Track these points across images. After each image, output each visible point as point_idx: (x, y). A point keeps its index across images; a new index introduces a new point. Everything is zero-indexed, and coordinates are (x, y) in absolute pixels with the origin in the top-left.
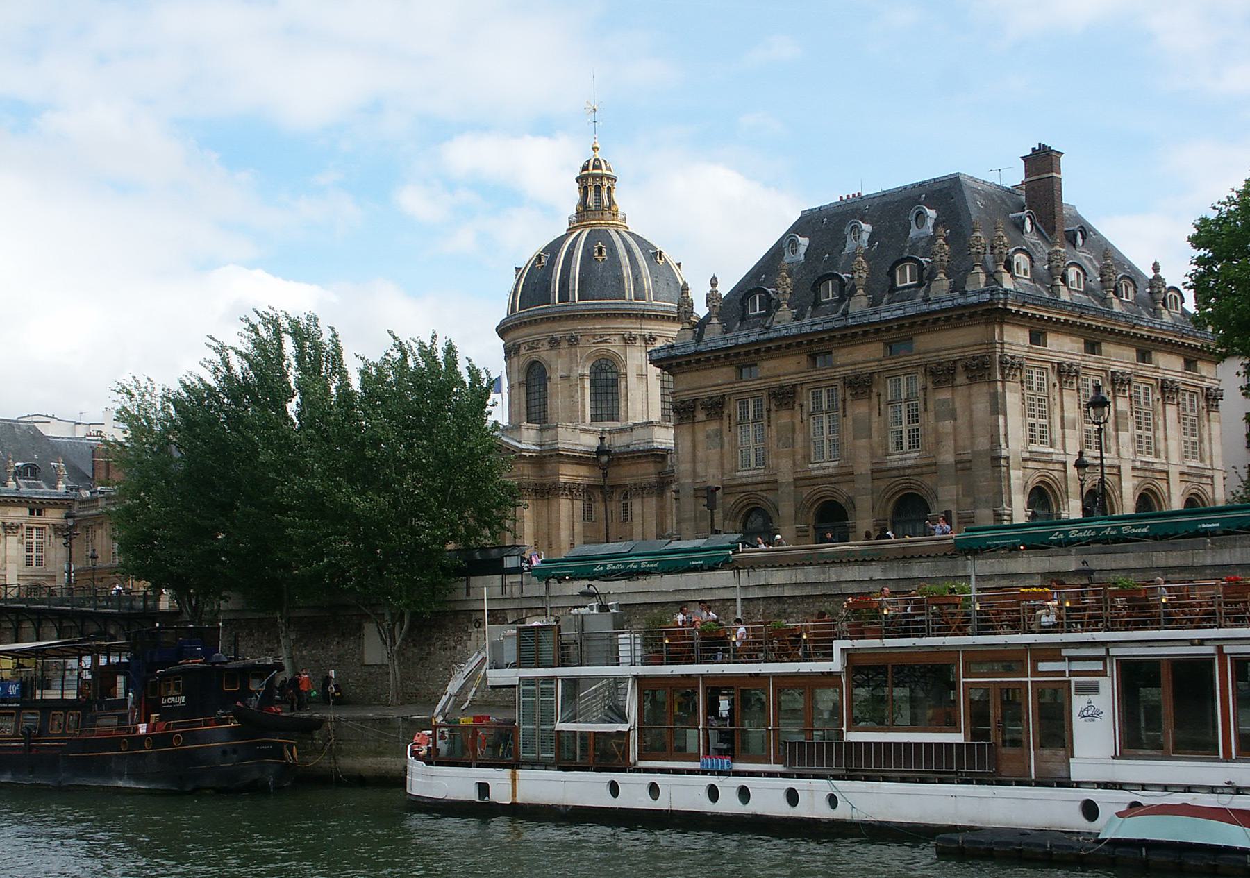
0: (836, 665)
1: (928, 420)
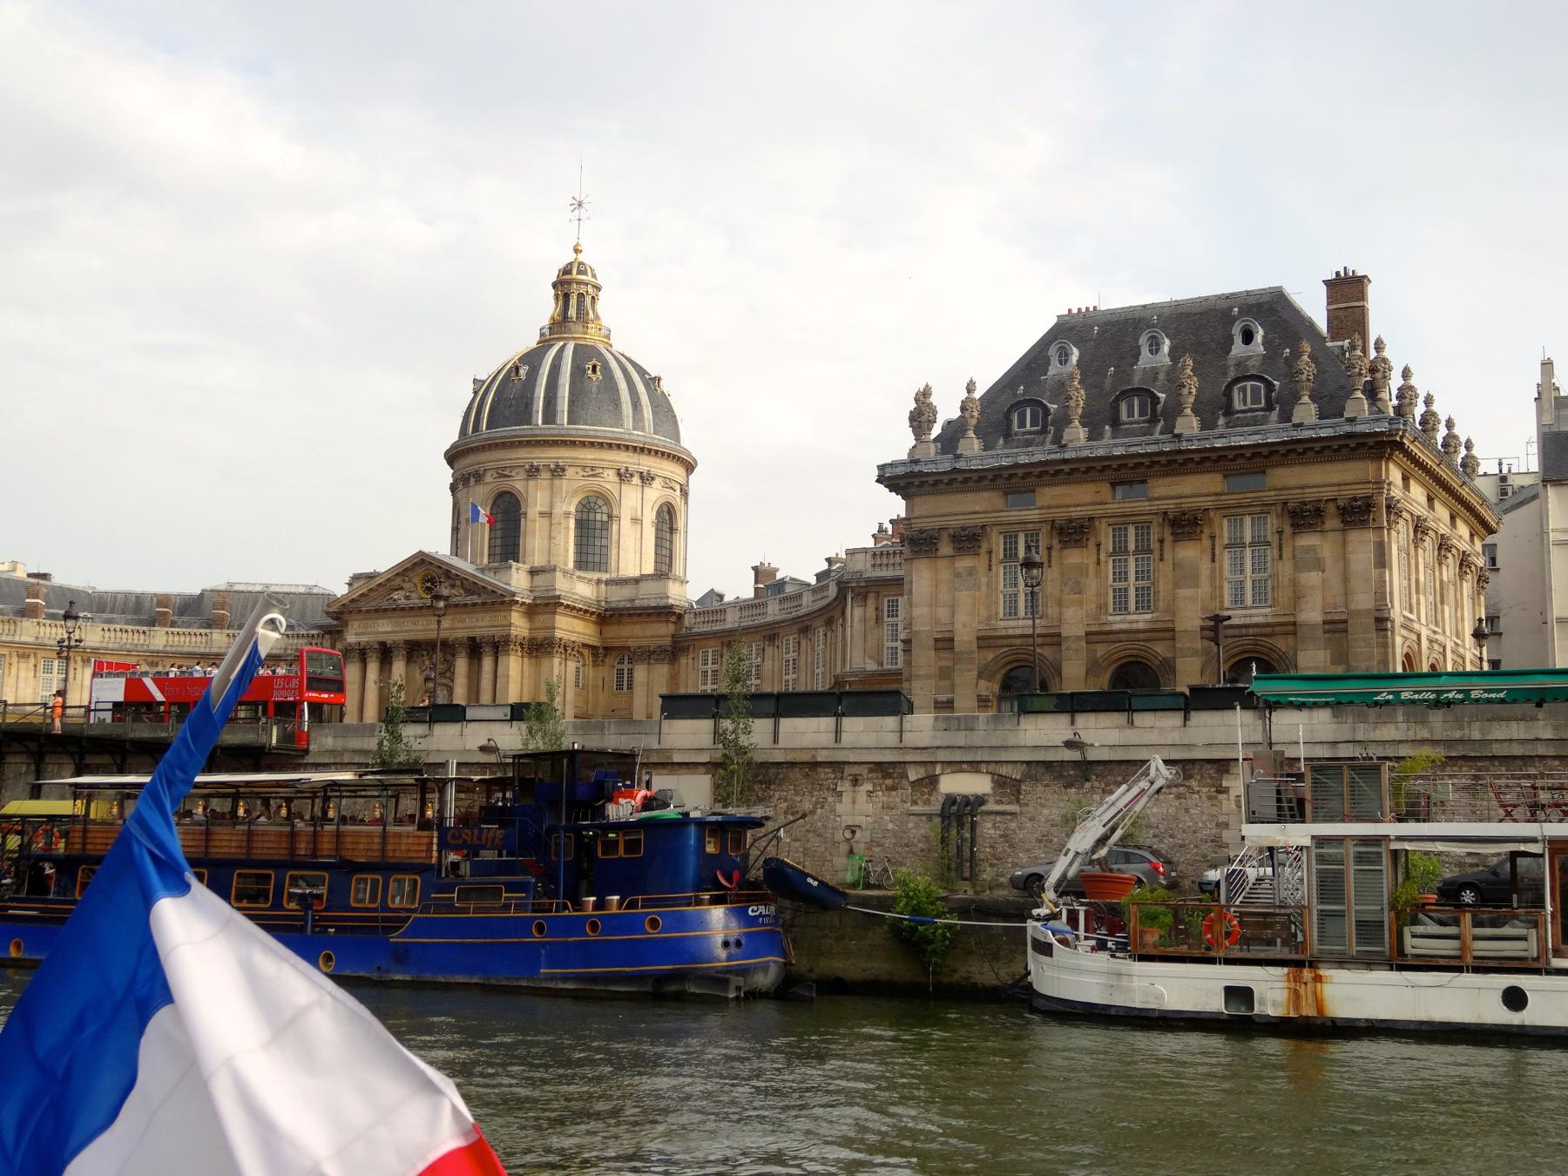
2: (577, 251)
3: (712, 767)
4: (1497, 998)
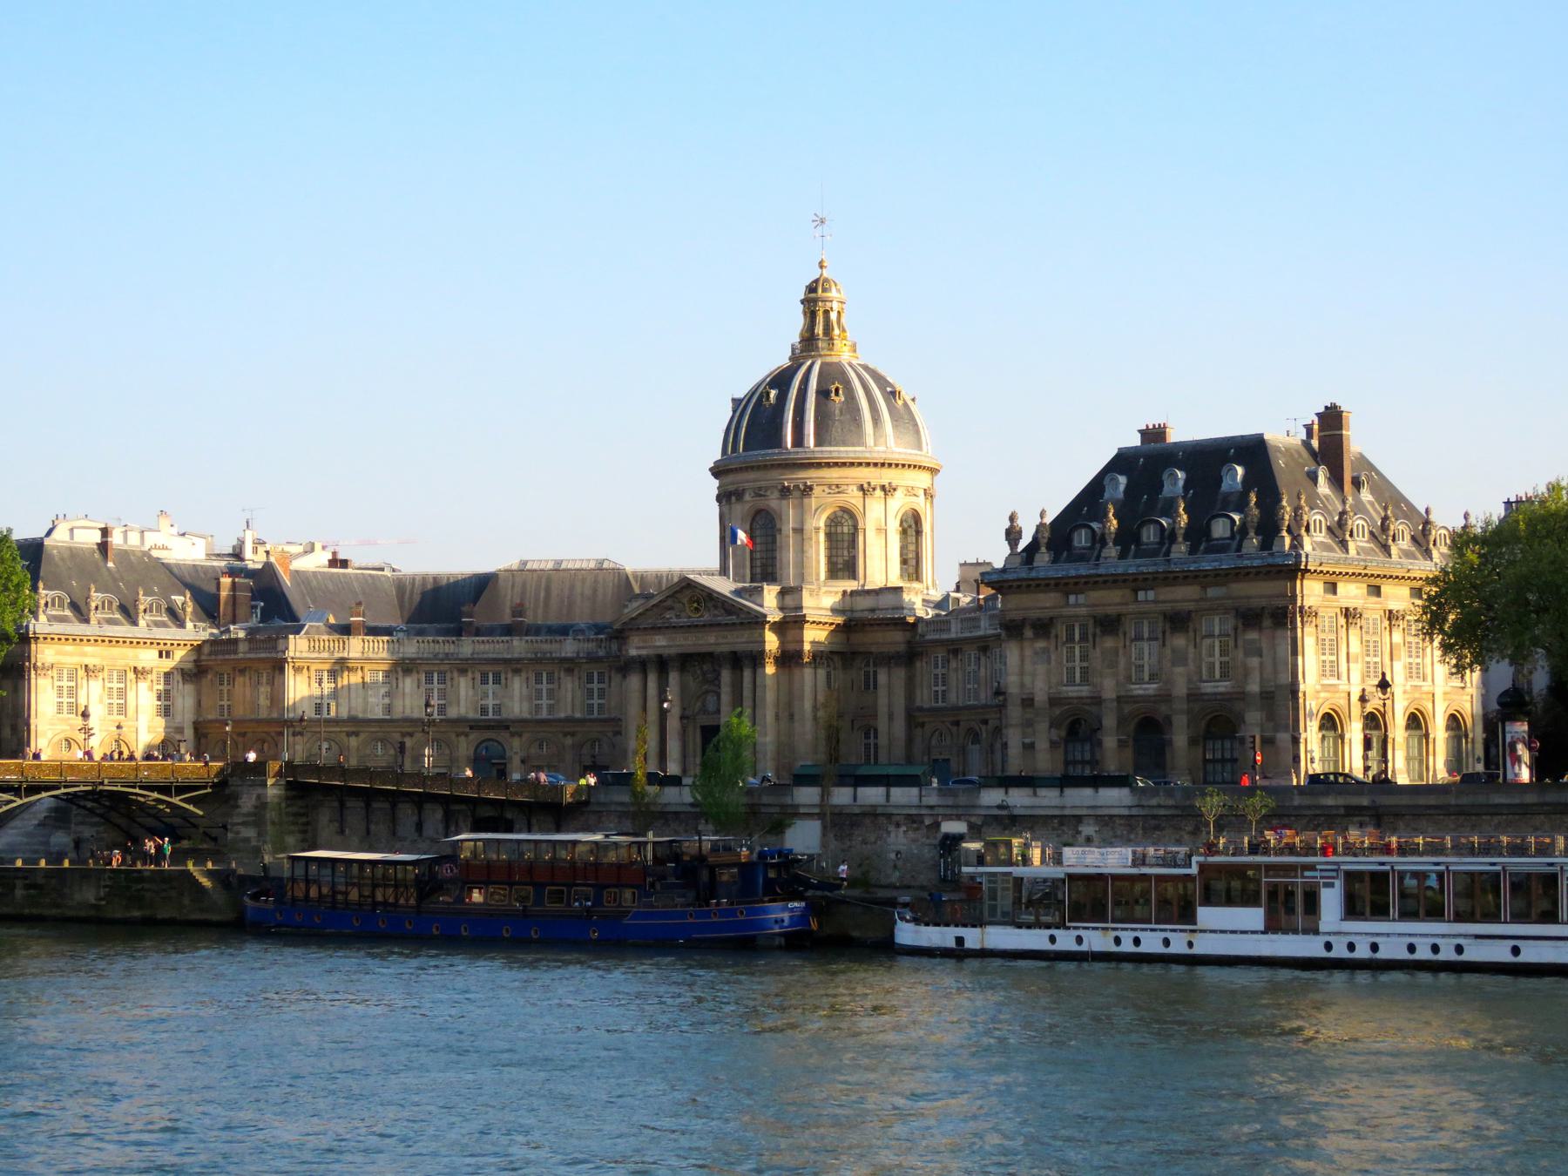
3: (821, 816)
4: (1442, 948)
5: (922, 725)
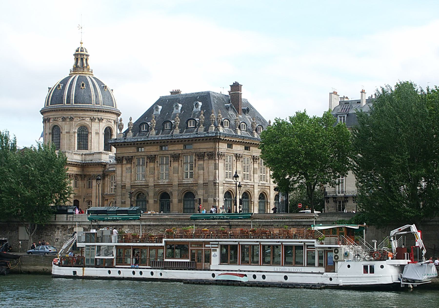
0: (163, 244)
1: (196, 170)
2: (81, 43)
5: (107, 200)
